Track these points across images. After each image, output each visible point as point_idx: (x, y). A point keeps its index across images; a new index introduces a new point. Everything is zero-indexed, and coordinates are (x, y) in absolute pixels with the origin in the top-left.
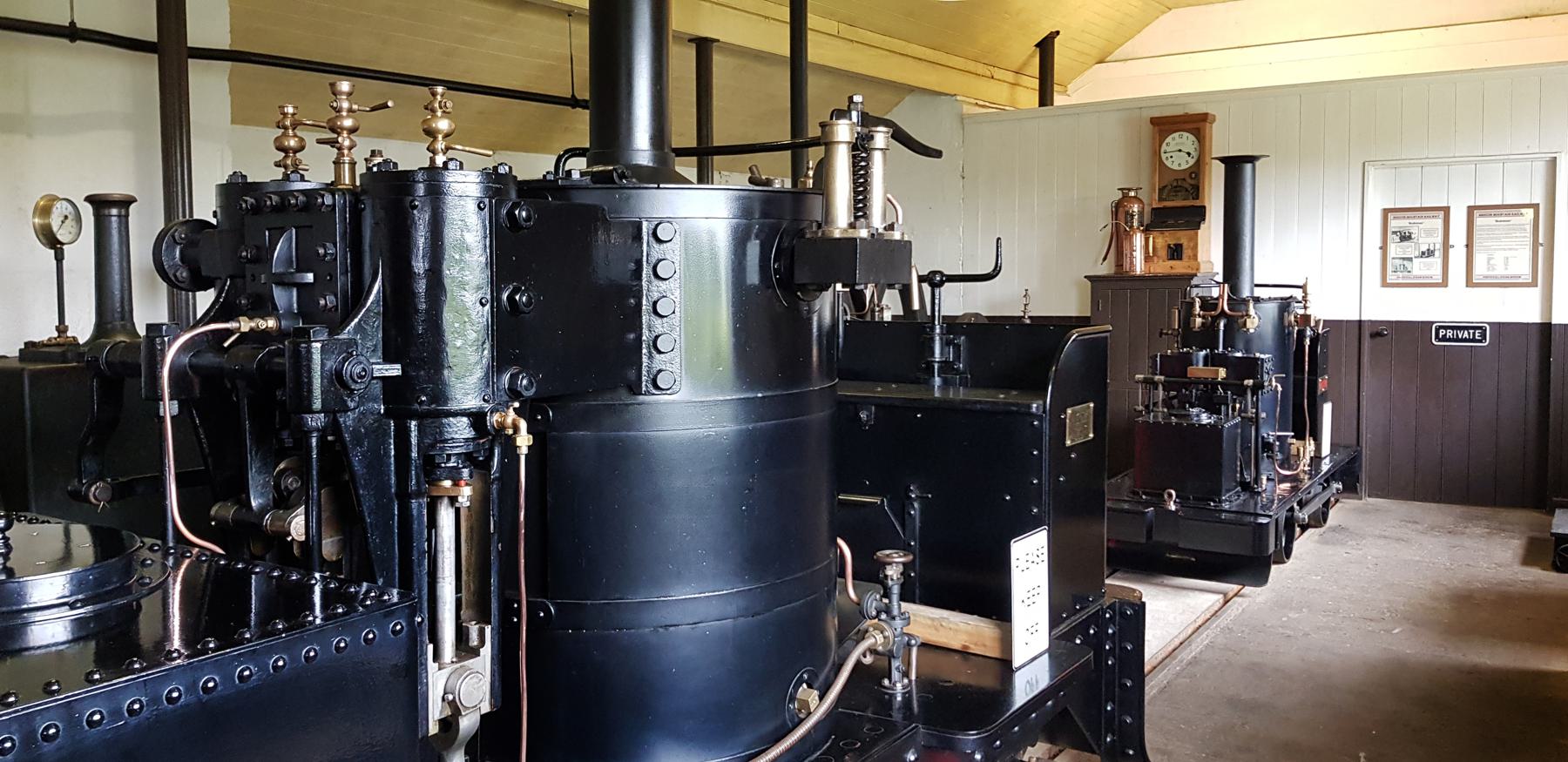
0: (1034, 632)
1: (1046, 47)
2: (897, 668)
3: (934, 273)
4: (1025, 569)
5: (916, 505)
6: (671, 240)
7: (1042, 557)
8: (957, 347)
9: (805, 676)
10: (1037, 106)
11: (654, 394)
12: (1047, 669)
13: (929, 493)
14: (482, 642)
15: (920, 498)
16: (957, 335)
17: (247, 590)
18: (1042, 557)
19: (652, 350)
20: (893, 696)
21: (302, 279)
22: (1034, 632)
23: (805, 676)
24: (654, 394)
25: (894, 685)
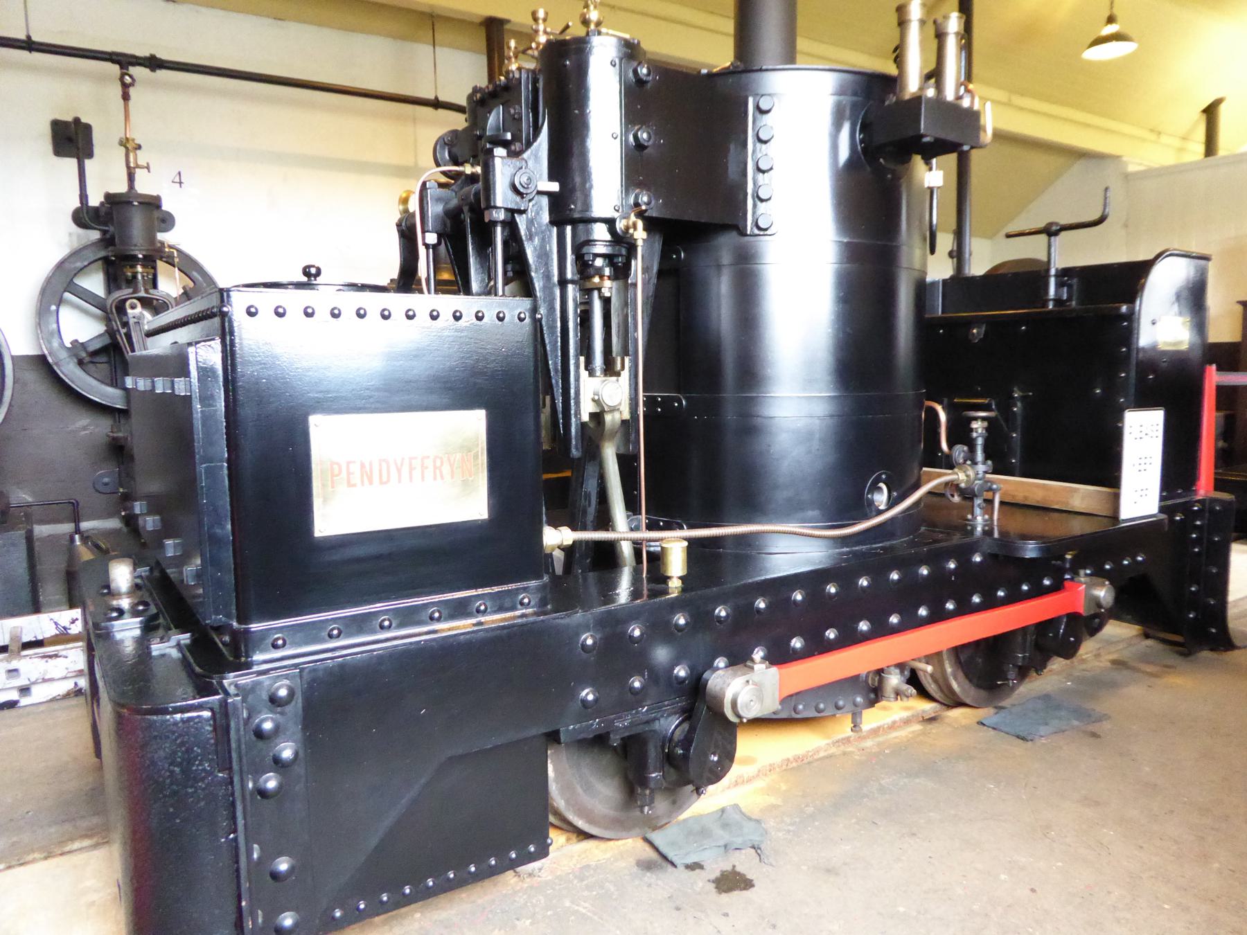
0: (1144, 495)
1: (1211, 112)
2: (979, 505)
3: (1051, 224)
4: (1138, 438)
5: (1019, 404)
6: (774, 105)
7: (1157, 434)
8: (1070, 287)
9: (884, 476)
10: (1203, 156)
11: (759, 235)
12: (1079, 145)
13: (1030, 392)
14: (623, 367)
15: (1023, 399)
16: (1070, 277)
17: (729, 747)
18: (1157, 434)
19: (756, 199)
20: (974, 528)
21: (589, 250)
22: (1144, 495)
23: (884, 476)
24: (759, 235)
25: (976, 518)
